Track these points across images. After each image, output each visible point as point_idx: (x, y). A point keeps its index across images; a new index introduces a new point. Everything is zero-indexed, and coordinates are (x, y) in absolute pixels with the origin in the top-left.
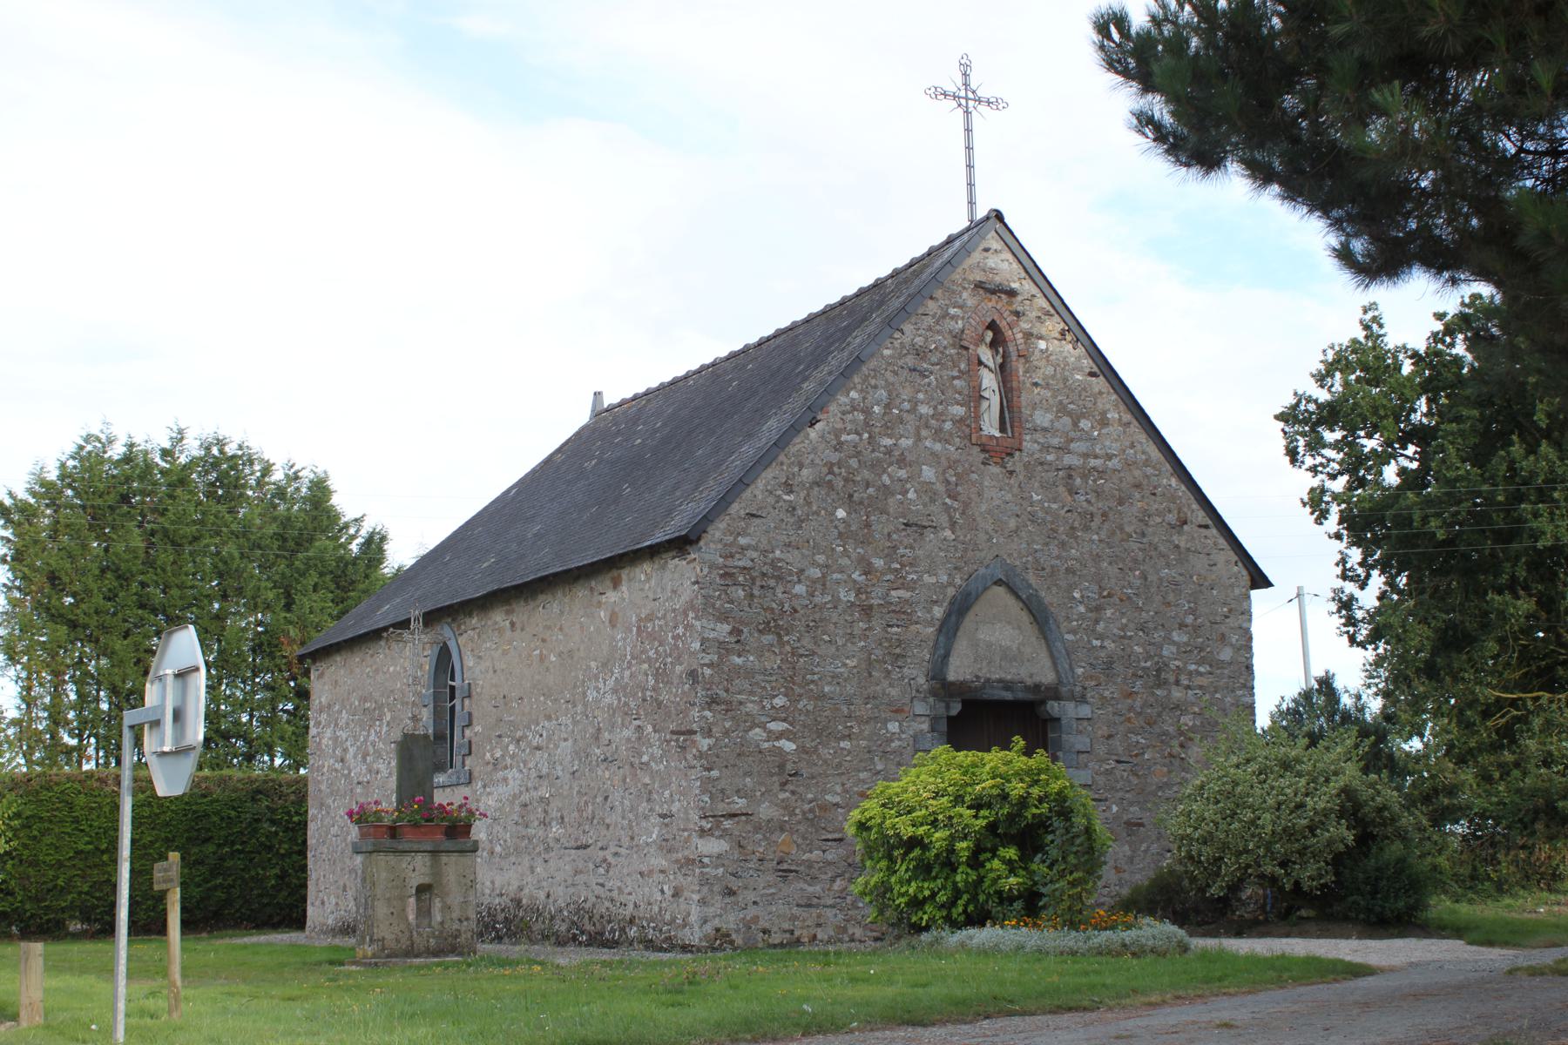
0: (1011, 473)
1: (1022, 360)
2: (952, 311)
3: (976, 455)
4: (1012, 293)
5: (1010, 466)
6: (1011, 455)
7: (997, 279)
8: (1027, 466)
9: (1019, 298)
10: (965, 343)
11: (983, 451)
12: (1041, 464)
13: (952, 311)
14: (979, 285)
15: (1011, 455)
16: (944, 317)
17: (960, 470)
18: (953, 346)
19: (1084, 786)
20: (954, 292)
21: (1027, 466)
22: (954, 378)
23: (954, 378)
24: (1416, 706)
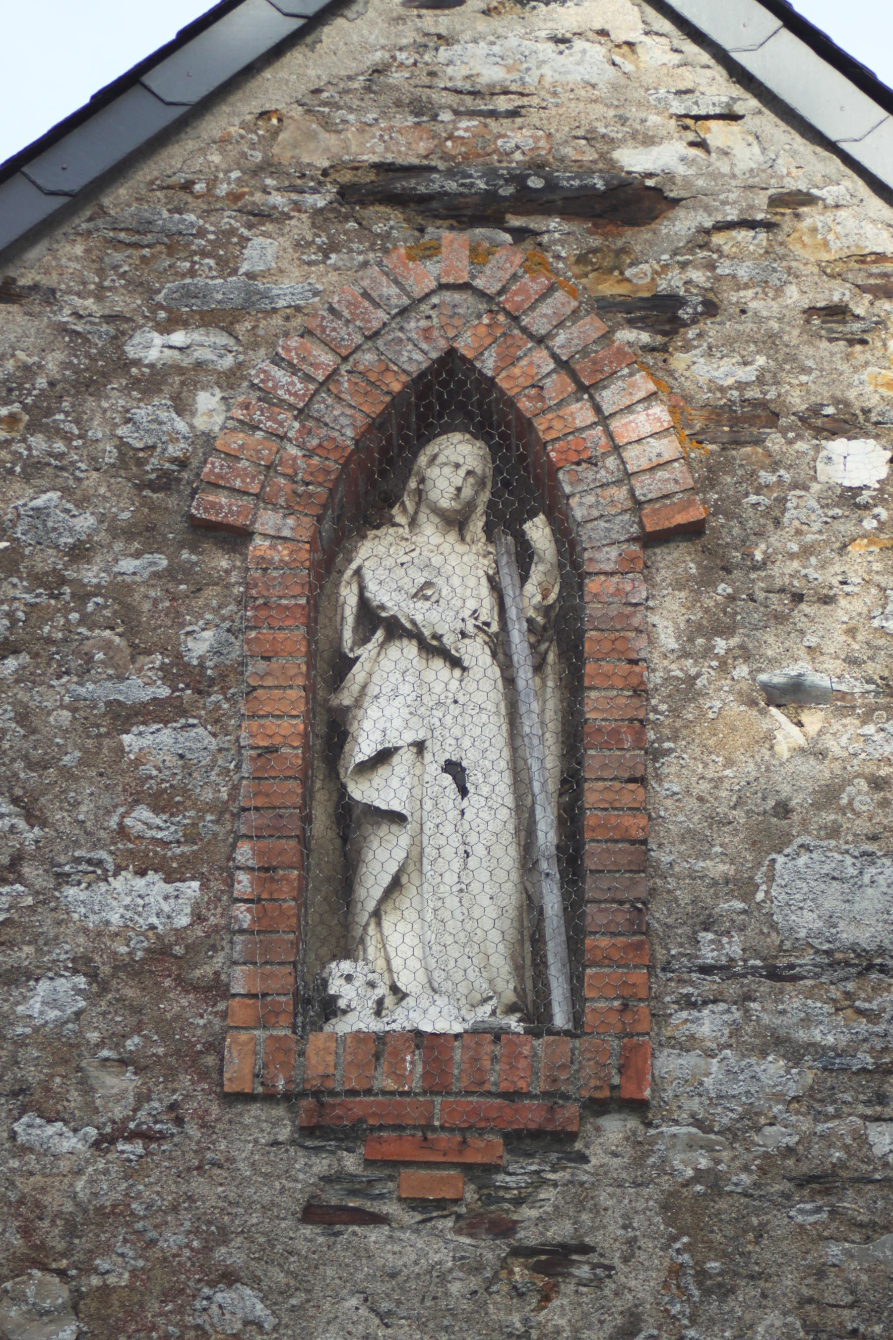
0: (554, 1260)
1: (679, 560)
2: (152, 347)
3: (262, 1164)
4: (631, 204)
5: (541, 1220)
6: (555, 1141)
7: (518, 140)
8: (687, 1210)
9: (682, 224)
10: (223, 506)
11: (316, 1132)
12: (820, 1183)
13: (152, 347)
14: (383, 191)
15: (555, 1141)
16: (88, 384)
17: (116, 1270)
18: (143, 534)
19: (220, 1307)
20: (175, 243)
21: (687, 1210)
22: (124, 716)
23: (124, 716)
24: (761, 656)
